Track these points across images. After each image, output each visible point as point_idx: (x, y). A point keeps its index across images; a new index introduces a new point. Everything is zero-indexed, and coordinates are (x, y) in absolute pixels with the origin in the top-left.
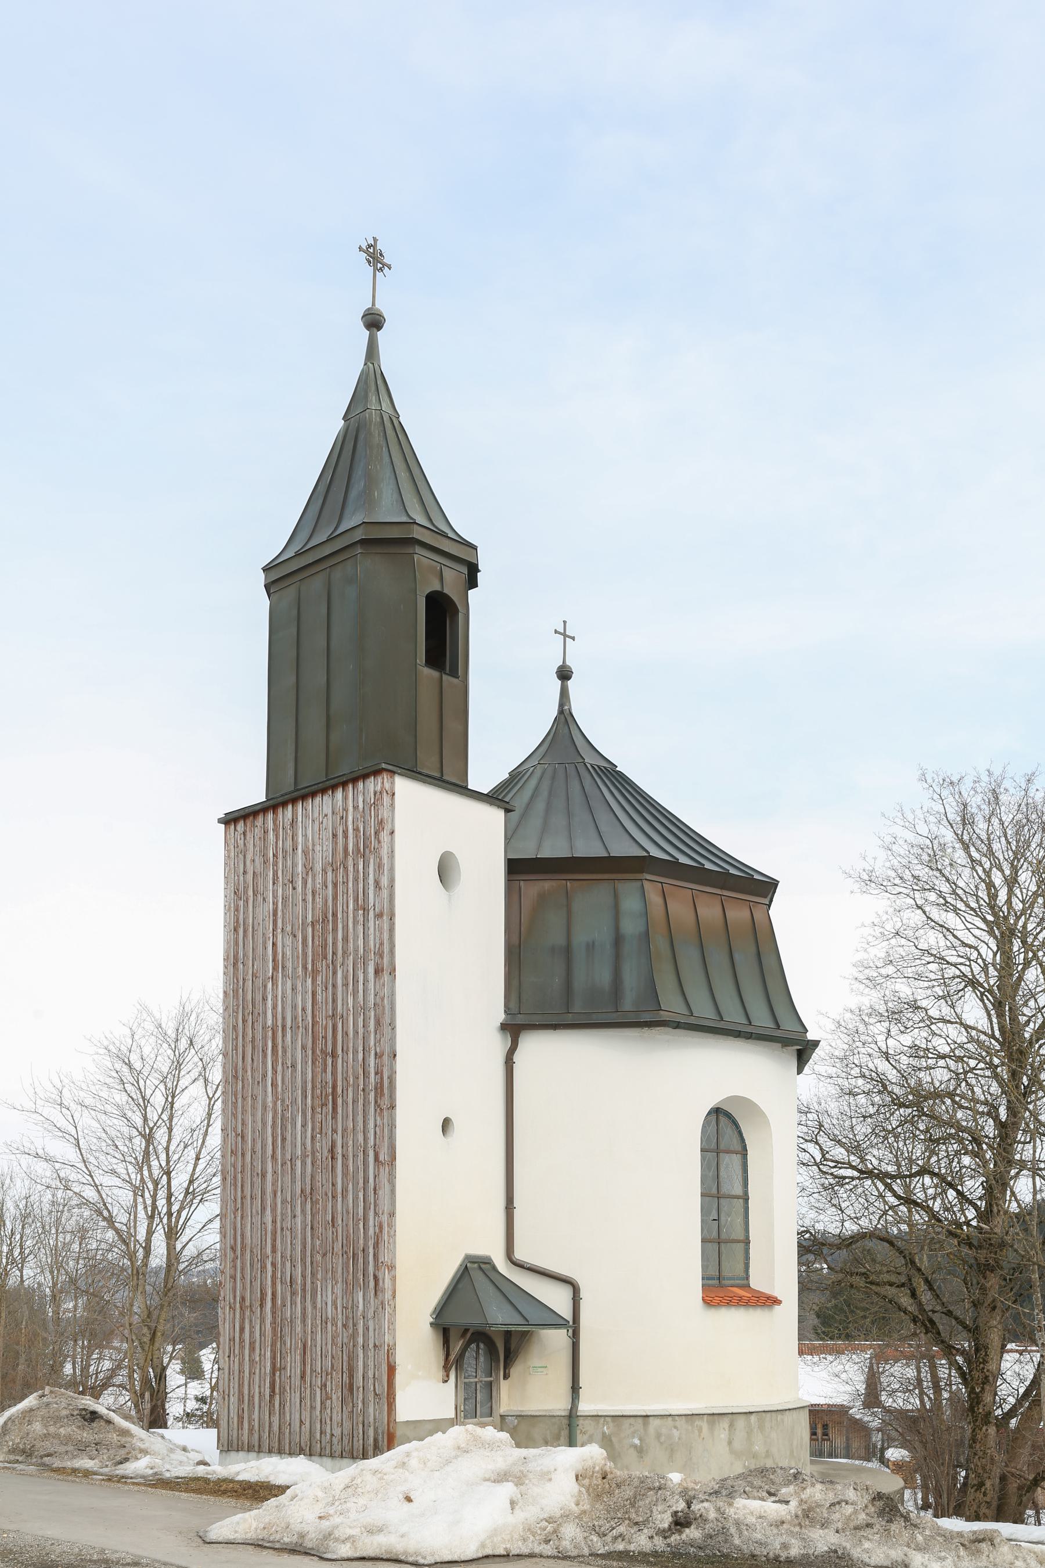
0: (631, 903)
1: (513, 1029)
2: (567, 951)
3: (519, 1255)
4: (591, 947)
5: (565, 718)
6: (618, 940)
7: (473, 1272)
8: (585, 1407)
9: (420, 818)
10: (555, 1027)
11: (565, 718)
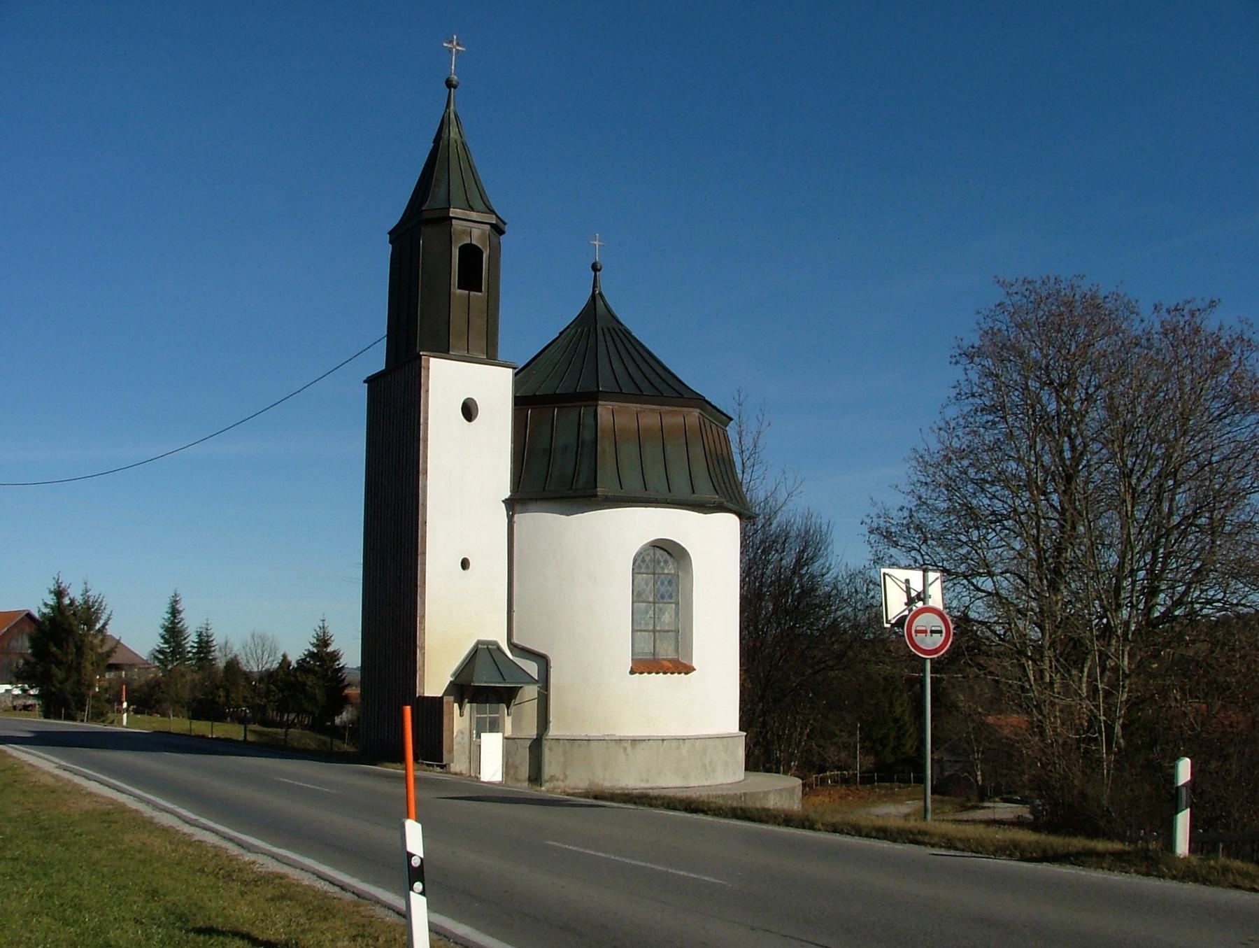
1: (513, 504)
3: (515, 641)
6: (579, 442)
7: (482, 653)
8: (553, 731)
10: (536, 500)
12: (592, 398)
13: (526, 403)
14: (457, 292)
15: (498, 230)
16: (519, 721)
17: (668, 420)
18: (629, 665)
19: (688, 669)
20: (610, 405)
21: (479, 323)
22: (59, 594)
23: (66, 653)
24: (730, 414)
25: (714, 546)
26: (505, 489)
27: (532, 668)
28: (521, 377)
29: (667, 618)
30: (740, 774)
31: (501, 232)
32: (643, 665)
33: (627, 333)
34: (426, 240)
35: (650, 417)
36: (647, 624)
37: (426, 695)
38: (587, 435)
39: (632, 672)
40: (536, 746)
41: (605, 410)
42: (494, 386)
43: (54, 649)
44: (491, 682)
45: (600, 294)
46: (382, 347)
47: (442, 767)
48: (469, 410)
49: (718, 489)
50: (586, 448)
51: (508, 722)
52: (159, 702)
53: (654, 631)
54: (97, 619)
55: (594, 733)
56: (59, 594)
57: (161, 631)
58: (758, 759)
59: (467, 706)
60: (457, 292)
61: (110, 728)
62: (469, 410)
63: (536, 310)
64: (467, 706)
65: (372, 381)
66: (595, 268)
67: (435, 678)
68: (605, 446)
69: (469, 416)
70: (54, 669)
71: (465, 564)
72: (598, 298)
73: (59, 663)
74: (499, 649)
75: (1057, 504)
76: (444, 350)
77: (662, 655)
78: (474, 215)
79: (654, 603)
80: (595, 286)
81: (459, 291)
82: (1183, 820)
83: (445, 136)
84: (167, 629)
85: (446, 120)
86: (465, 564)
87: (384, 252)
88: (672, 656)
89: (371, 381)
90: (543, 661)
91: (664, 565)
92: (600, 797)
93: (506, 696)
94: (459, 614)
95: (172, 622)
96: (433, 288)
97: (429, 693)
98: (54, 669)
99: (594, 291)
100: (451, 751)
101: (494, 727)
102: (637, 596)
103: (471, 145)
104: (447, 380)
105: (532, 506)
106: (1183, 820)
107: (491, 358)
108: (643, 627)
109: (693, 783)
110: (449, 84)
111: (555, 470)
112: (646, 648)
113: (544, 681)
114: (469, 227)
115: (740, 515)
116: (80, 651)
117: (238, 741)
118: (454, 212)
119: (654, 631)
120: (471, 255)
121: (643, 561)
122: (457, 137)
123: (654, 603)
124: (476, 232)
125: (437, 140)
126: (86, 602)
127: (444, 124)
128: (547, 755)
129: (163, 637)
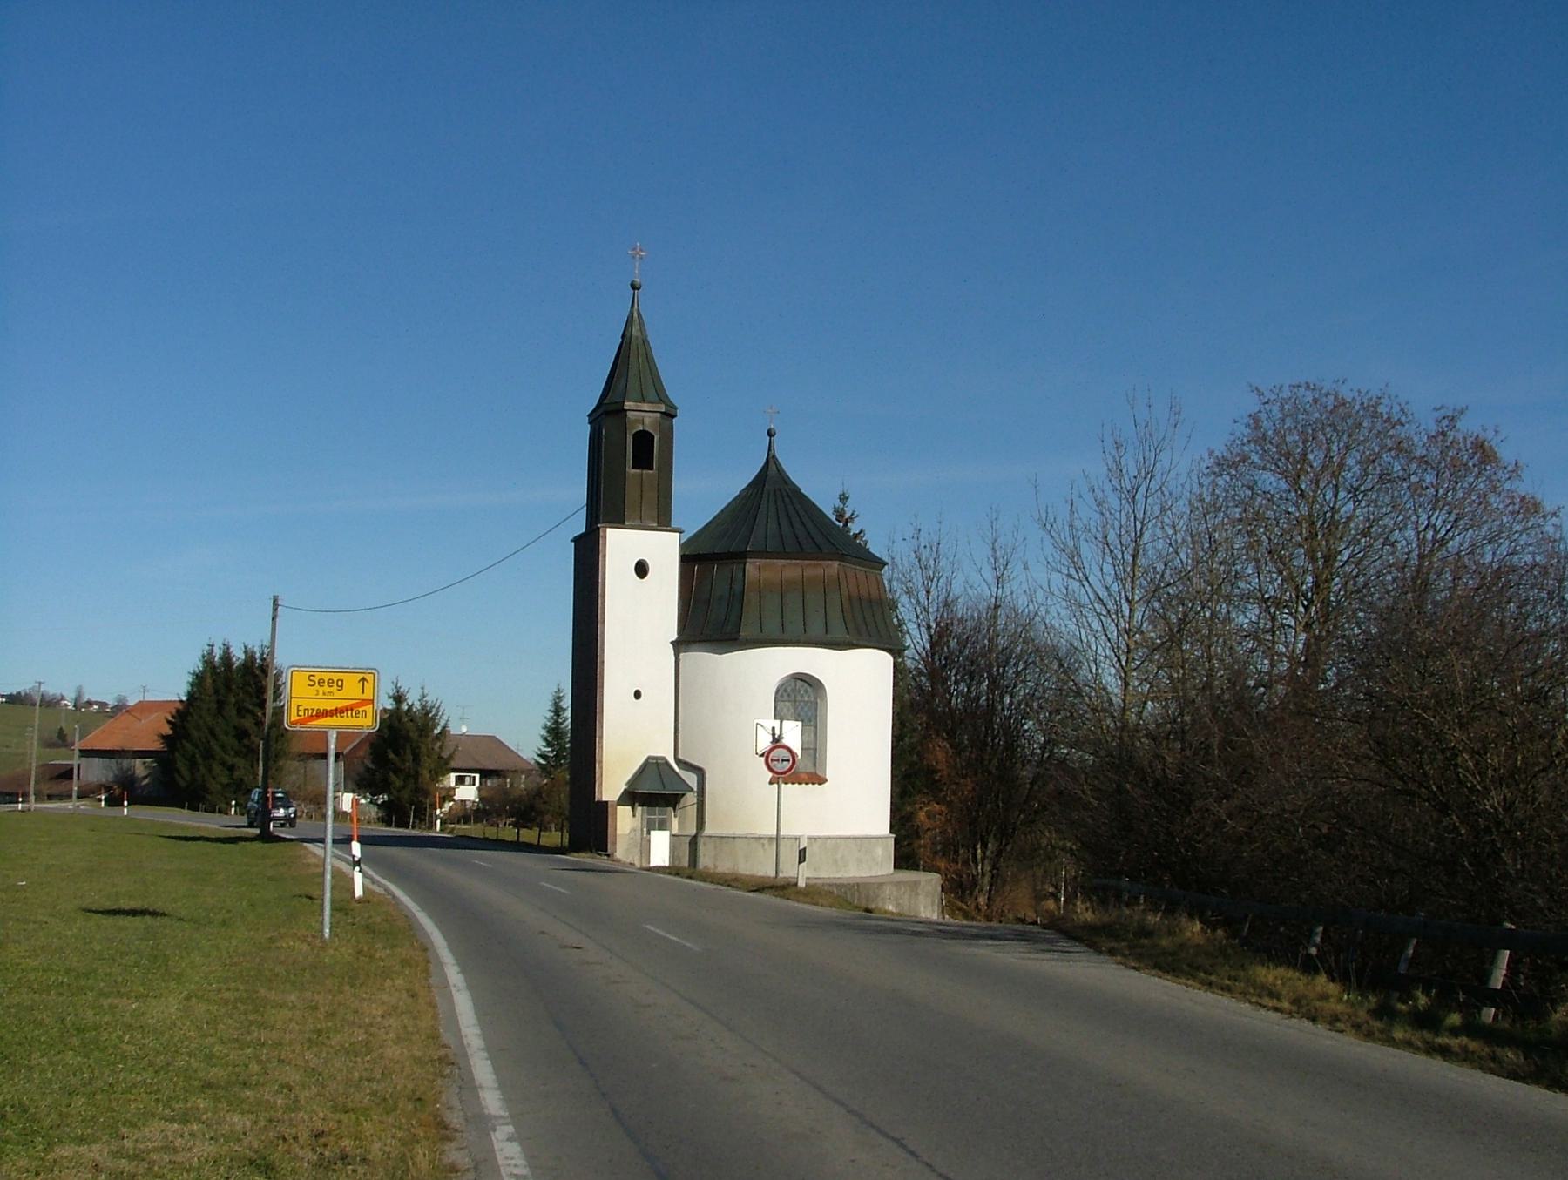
1: (679, 645)
5: (771, 459)
7: (654, 766)
8: (708, 830)
9: (621, 546)
11: (771, 459)
12: (741, 556)
13: (690, 559)
14: (631, 471)
15: (669, 415)
16: (681, 821)
17: (809, 572)
19: (821, 781)
20: (759, 562)
21: (650, 495)
22: (399, 698)
23: (403, 761)
24: (886, 559)
26: (670, 627)
27: (691, 779)
28: (683, 546)
30: (889, 867)
31: (673, 416)
33: (796, 491)
35: (791, 570)
38: (737, 588)
40: (694, 842)
41: (752, 567)
42: (662, 549)
43: (392, 756)
44: (657, 791)
48: (641, 569)
49: (865, 624)
50: (736, 599)
51: (675, 822)
52: (541, 813)
54: (435, 727)
55: (739, 833)
56: (399, 698)
57: (544, 732)
58: (904, 859)
59: (639, 809)
60: (631, 471)
61: (425, 833)
62: (641, 569)
63: (706, 485)
65: (576, 540)
66: (771, 434)
67: (611, 786)
68: (751, 597)
69: (644, 576)
70: (393, 777)
71: (637, 695)
73: (397, 771)
74: (667, 763)
75: (217, 768)
76: (619, 521)
77: (796, 769)
78: (645, 407)
84: (550, 730)
86: (637, 695)
88: (810, 769)
90: (700, 772)
91: (801, 696)
92: (732, 881)
93: (672, 801)
94: (630, 737)
95: (556, 722)
96: (624, 466)
98: (393, 777)
100: (614, 843)
101: (662, 826)
104: (621, 546)
105: (694, 646)
107: (663, 522)
109: (823, 875)
110: (634, 287)
111: (714, 614)
113: (701, 792)
114: (641, 415)
115: (889, 651)
116: (416, 758)
117: (664, 868)
118: (628, 405)
120: (644, 439)
124: (647, 421)
125: (623, 336)
126: (424, 707)
127: (630, 322)
128: (702, 849)
129: (545, 739)
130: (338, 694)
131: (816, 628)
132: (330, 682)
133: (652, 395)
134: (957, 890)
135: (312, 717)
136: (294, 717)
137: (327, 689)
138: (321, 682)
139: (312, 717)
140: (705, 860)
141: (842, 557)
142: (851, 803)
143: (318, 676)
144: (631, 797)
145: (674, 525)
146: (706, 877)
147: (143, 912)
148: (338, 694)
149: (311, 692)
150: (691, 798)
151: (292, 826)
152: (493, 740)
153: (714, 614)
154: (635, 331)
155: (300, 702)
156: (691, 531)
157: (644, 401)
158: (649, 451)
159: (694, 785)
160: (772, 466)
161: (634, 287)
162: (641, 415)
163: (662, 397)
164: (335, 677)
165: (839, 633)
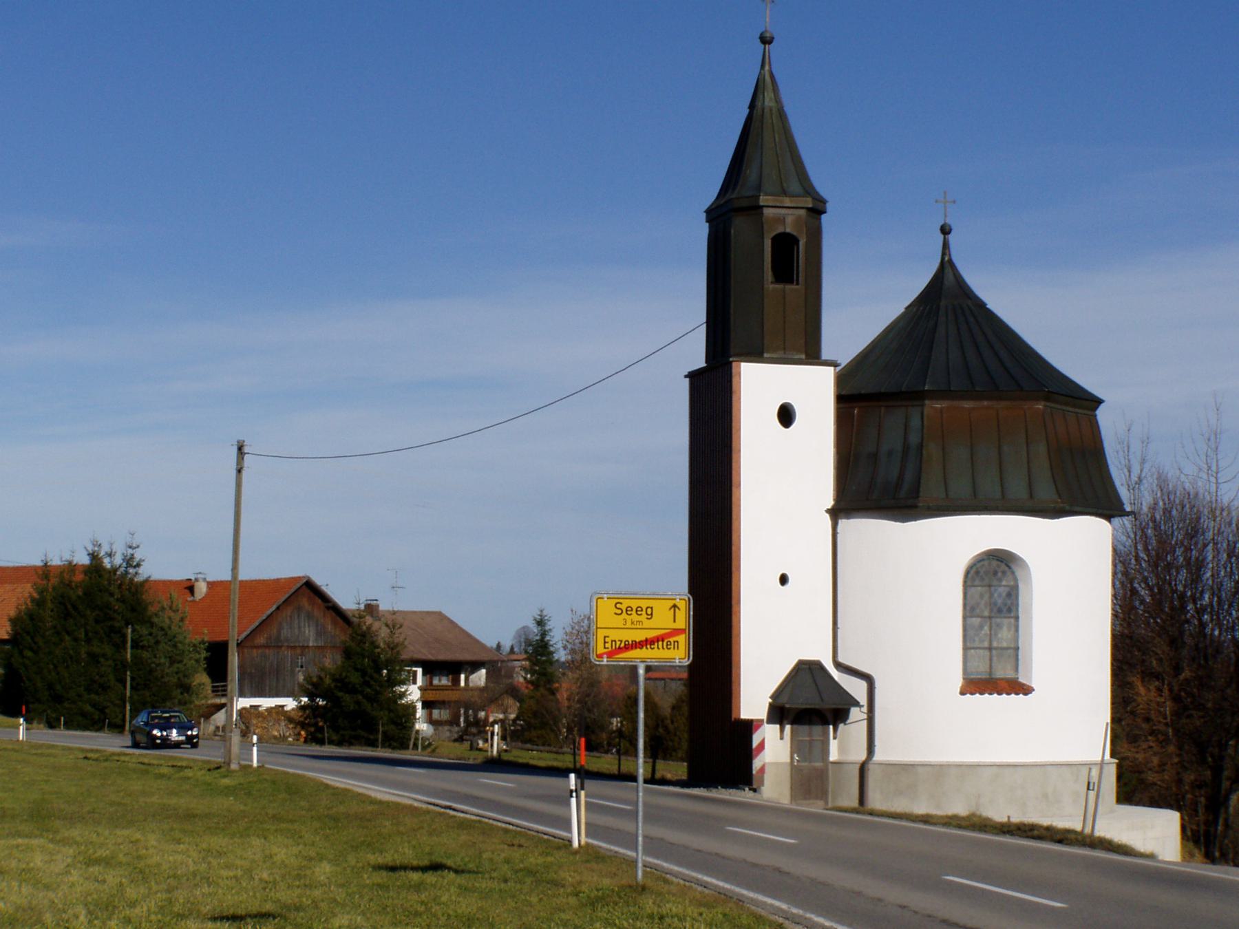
0: (915, 422)
1: (837, 512)
2: (874, 457)
3: (841, 659)
4: (890, 453)
5: (946, 265)
6: (906, 449)
7: (807, 671)
8: (878, 757)
9: (759, 385)
11: (946, 265)
15: (817, 210)
18: (958, 682)
19: (1026, 690)
25: (1070, 566)
26: (827, 496)
27: (856, 688)
28: (841, 380)
29: (1005, 635)
32: (976, 685)
33: (981, 305)
34: (740, 226)
36: (982, 641)
37: (743, 717)
39: (962, 693)
42: (813, 388)
44: (814, 702)
45: (950, 261)
46: (701, 335)
47: (755, 790)
48: (786, 415)
49: (1076, 482)
53: (990, 649)
62: (786, 415)
63: (862, 303)
64: (788, 728)
65: (693, 376)
66: (946, 230)
67: (753, 698)
69: (788, 425)
71: (784, 580)
72: (947, 265)
76: (756, 355)
77: (994, 672)
78: (787, 202)
79: (990, 618)
80: (943, 254)
81: (771, 286)
82: (255, 749)
83: (759, 104)
85: (761, 84)
87: (702, 231)
89: (693, 376)
91: (994, 586)
96: (757, 282)
97: (745, 714)
99: (943, 259)
102: (969, 610)
103: (789, 109)
104: (759, 385)
106: (255, 749)
107: (812, 355)
108: (977, 644)
111: (876, 481)
112: (980, 668)
114: (782, 214)
118: (763, 200)
119: (990, 649)
120: (785, 245)
121: (977, 573)
122: (773, 104)
123: (990, 618)
124: (789, 220)
125: (752, 106)
130: (647, 623)
131: (1017, 489)
132: (639, 610)
133: (795, 187)
134: (1202, 838)
135: (620, 650)
136: (601, 650)
137: (635, 617)
138: (629, 609)
139: (620, 650)
140: (876, 800)
141: (1048, 397)
142: (1056, 724)
143: (626, 603)
144: (778, 713)
145: (825, 355)
146: (871, 813)
147: (393, 869)
148: (647, 623)
149: (618, 621)
150: (856, 714)
151: (195, 746)
152: (440, 616)
153: (876, 481)
154: (768, 100)
155: (606, 632)
156: (844, 360)
157: (784, 193)
158: (795, 261)
159: (862, 697)
160: (948, 270)
161: (766, 40)
162: (782, 214)
163: (808, 190)
164: (644, 604)
165: (1045, 491)
